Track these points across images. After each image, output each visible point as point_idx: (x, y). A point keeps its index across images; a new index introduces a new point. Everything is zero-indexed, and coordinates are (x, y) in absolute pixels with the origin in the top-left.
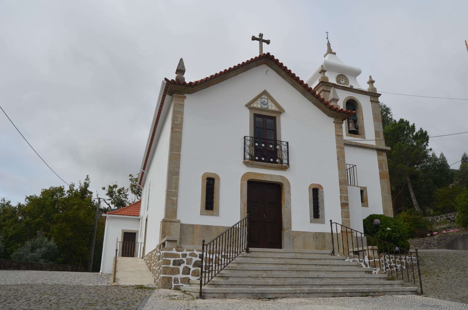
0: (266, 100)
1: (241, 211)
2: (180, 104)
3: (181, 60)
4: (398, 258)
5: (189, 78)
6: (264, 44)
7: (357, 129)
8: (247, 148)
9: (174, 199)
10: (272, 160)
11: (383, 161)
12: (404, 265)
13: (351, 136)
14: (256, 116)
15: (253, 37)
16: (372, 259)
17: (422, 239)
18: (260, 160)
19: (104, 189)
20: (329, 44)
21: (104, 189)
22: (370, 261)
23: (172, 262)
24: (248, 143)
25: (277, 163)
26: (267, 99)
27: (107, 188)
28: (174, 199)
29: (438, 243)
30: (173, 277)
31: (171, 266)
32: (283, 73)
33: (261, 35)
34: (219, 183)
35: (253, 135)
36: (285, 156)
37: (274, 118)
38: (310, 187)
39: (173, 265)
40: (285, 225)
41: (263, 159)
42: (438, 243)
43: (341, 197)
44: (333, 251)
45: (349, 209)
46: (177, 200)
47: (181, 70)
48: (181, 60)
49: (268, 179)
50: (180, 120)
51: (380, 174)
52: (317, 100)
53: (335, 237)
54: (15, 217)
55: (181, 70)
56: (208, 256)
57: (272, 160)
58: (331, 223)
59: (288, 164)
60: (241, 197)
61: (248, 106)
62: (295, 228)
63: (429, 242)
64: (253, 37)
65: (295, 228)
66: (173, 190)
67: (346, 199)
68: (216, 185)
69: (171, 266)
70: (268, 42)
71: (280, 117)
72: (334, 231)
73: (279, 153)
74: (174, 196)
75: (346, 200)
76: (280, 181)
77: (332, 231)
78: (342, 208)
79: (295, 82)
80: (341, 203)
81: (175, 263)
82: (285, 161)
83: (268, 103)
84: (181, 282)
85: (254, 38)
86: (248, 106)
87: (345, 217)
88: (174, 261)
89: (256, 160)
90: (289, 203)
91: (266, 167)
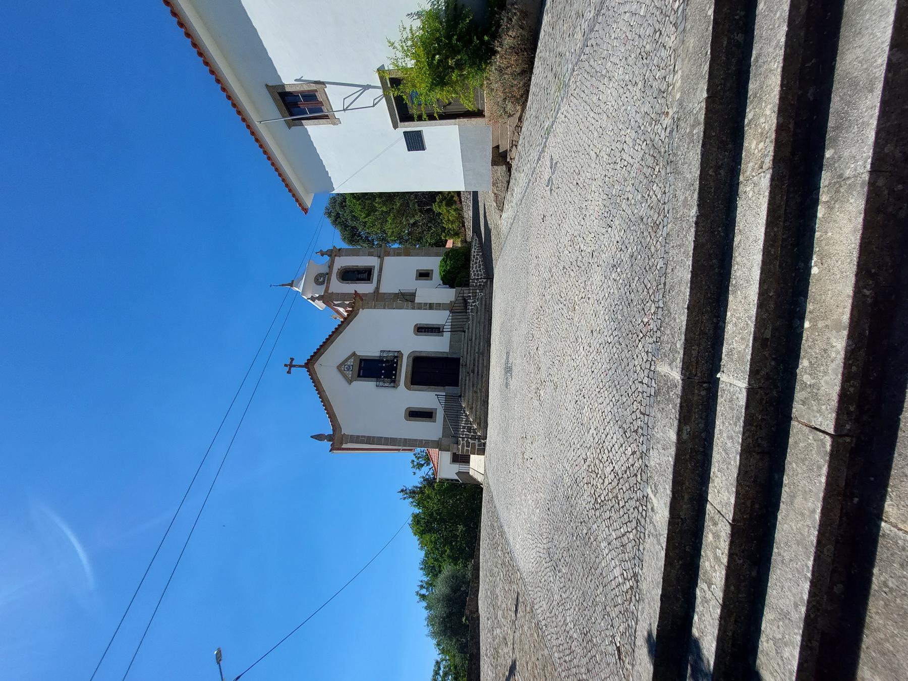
3: (312, 437)
5: (329, 431)
6: (294, 363)
8: (386, 385)
9: (424, 442)
10: (395, 365)
13: (372, 279)
14: (359, 376)
15: (288, 372)
18: (395, 375)
19: (415, 473)
21: (415, 473)
23: (467, 448)
24: (381, 384)
25: (397, 360)
26: (345, 365)
27: (414, 470)
28: (424, 442)
30: (477, 447)
31: (469, 449)
32: (322, 350)
33: (286, 365)
35: (376, 379)
38: (416, 335)
39: (469, 447)
40: (445, 356)
43: (424, 309)
46: (424, 440)
47: (319, 437)
49: (410, 368)
50: (363, 438)
51: (405, 256)
53: (446, 404)
54: (470, 243)
55: (319, 437)
56: (464, 422)
57: (395, 365)
59: (398, 352)
61: (350, 382)
64: (288, 372)
68: (413, 410)
69: (469, 449)
70: (292, 359)
72: (450, 330)
73: (389, 359)
74: (422, 443)
78: (433, 309)
80: (429, 309)
81: (468, 446)
82: (396, 354)
85: (289, 372)
88: (467, 447)
89: (395, 378)
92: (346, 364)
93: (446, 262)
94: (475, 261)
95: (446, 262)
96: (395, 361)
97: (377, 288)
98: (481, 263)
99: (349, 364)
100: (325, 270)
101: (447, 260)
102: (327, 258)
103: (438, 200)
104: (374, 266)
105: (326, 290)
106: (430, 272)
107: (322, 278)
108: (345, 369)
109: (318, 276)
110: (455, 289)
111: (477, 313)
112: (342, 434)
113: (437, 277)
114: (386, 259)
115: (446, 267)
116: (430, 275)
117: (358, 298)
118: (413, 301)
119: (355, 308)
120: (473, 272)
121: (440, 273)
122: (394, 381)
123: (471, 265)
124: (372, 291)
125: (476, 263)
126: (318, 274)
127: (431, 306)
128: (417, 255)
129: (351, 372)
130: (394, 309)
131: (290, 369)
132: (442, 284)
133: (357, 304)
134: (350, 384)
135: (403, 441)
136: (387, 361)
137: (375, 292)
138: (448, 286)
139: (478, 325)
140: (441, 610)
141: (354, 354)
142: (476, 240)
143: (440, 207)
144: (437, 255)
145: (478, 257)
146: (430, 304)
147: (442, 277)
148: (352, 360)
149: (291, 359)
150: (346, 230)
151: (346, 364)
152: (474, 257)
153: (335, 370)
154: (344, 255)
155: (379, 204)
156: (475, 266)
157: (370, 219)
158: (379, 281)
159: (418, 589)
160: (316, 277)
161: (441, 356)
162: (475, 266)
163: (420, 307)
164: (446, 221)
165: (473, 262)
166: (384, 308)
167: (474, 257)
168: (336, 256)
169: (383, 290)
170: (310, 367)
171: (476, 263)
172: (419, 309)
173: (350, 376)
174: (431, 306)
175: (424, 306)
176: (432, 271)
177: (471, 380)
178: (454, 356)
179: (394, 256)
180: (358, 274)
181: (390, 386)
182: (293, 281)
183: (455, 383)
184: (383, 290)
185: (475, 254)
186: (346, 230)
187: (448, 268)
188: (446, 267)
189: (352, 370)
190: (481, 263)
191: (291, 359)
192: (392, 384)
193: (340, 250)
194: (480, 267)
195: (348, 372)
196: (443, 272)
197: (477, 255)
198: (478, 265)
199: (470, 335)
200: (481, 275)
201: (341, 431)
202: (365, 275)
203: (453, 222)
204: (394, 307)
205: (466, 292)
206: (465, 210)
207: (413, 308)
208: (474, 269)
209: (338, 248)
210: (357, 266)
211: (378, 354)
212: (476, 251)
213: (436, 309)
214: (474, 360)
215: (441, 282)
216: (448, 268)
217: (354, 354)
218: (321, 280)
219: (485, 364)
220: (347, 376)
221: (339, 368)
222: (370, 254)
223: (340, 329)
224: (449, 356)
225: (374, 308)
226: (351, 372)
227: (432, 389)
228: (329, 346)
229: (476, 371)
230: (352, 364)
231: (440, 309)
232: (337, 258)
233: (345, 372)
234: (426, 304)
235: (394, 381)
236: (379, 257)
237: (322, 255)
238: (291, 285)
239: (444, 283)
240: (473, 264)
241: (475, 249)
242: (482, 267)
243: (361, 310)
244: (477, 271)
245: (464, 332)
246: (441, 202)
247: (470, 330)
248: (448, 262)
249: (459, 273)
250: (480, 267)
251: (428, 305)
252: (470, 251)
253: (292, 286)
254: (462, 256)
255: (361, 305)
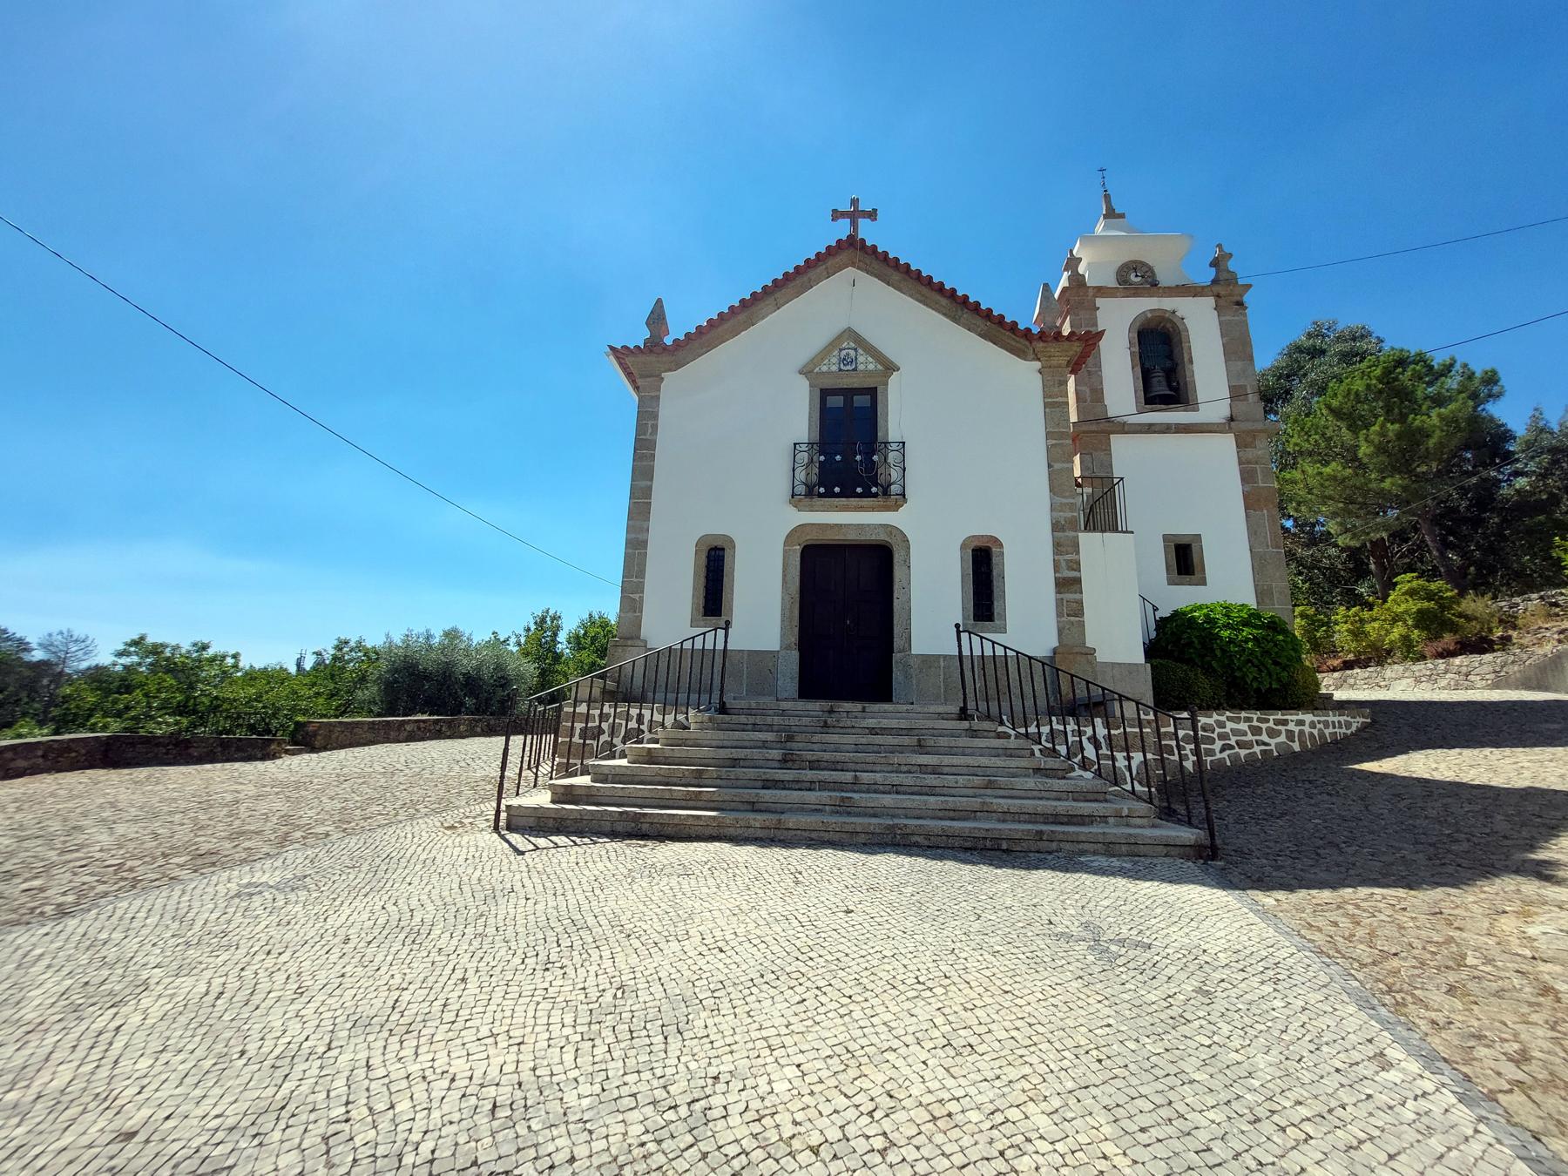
0: (852, 353)
1: (783, 615)
2: (652, 397)
3: (659, 301)
4: (1272, 722)
7: (1177, 390)
9: (636, 596)
11: (1257, 463)
12: (1296, 739)
14: (825, 393)
15: (835, 211)
16: (1119, 728)
17: (1441, 661)
18: (830, 494)
20: (1107, 197)
22: (1112, 732)
24: (803, 457)
25: (875, 495)
26: (855, 350)
28: (636, 596)
29: (1495, 672)
32: (896, 276)
33: (855, 202)
34: (734, 556)
35: (816, 437)
36: (895, 475)
37: (872, 392)
38: (963, 546)
40: (898, 643)
41: (859, 490)
42: (1495, 672)
44: (961, 709)
45: (1081, 593)
46: (641, 598)
48: (659, 301)
49: (852, 537)
51: (1246, 497)
52: (989, 323)
58: (959, 633)
60: (784, 581)
61: (806, 371)
62: (918, 648)
63: (1464, 670)
64: (835, 211)
65: (918, 648)
66: (634, 580)
67: (1075, 567)
70: (872, 215)
71: (886, 384)
72: (966, 652)
75: (1073, 570)
76: (882, 537)
77: (960, 652)
78: (1058, 592)
79: (925, 290)
82: (894, 489)
83: (856, 359)
84: (1261, 728)
86: (806, 371)
87: (1068, 615)
89: (820, 496)
90: (907, 587)
91: (846, 509)
92: (860, 351)
93: (1246, 623)
94: (1264, 726)
95: (1246, 623)
96: (874, 490)
97: (1125, 429)
98: (1257, 749)
99: (861, 359)
100: (1165, 279)
101: (1256, 627)
102: (1206, 276)
103: (1433, 586)
104: (1203, 582)
105: (1102, 291)
106: (1198, 575)
107: (1139, 279)
108: (844, 352)
109: (1145, 269)
110: (1142, 660)
111: (1037, 770)
112: (663, 375)
113: (1184, 598)
114: (1227, 443)
115: (1227, 626)
116: (1188, 578)
117: (1077, 348)
118: (1092, 525)
119: (1040, 345)
120: (1217, 722)
121: (1200, 608)
122: (810, 492)
123: (1243, 714)
124: (1112, 412)
125: (1256, 731)
126: (1151, 269)
127: (1068, 585)
128: (1253, 532)
129: (834, 368)
130: (1050, 466)
131: (844, 215)
132: (1159, 615)
133: (1053, 348)
134: (801, 373)
135: (640, 537)
136: (872, 466)
137: (1108, 419)
138: (1153, 635)
139: (977, 780)
140: (428, 663)
141: (890, 368)
142: (1349, 726)
143: (1412, 593)
144: (1262, 593)
145: (1282, 738)
146: (1078, 581)
147: (1184, 614)
148: (871, 367)
149: (875, 210)
150: (1279, 378)
151: (860, 351)
152: (1277, 722)
153: (843, 325)
154: (1223, 318)
155: (1383, 434)
156: (1244, 726)
157: (1325, 419)
158: (1150, 429)
159: (551, 613)
160: (1141, 262)
161: (897, 629)
162: (1244, 726)
163: (1065, 549)
164: (1356, 615)
165: (1259, 720)
166: (1049, 435)
167: (1277, 722)
168: (1218, 296)
169: (1118, 443)
170: (843, 257)
171: (1256, 731)
172: (1058, 547)
173: (825, 369)
174: (1068, 585)
175: (1067, 561)
176: (1203, 582)
177: (756, 754)
178: (897, 675)
179: (1240, 463)
180: (1163, 370)
181: (796, 483)
182: (1122, 216)
183: (810, 687)
184: (1118, 443)
185: (1291, 726)
186: (1279, 378)
187: (1225, 633)
188: (1227, 626)
189: (840, 370)
190: (1257, 749)
191: (875, 210)
192: (801, 489)
193: (1240, 304)
194: (1240, 744)
195: (834, 360)
196: (1207, 616)
197: (1290, 735)
198: (1250, 737)
199: (943, 741)
200: (1211, 752)
201: (670, 370)
202: (1161, 388)
203: (1357, 634)
204: (1057, 466)
205: (1136, 713)
206: (1415, 668)
207: (1056, 527)
208: (1230, 725)
209: (1245, 299)
210: (1191, 362)
211: (893, 435)
212: (1307, 729)
213: (1059, 603)
214: (835, 766)
215: (1165, 612)
216: (1225, 633)
217: (890, 368)
218: (1132, 277)
219: (792, 820)
220: (823, 359)
221: (851, 334)
222: (1236, 394)
223: (967, 315)
224: (896, 657)
225: (1046, 405)
226: (834, 368)
227: (791, 612)
228: (911, 296)
229: (787, 775)
230: (861, 367)
231: (1059, 614)
232: (1211, 301)
233: (836, 353)
234: (1075, 565)
235: (810, 492)
236: (1232, 419)
237: (1215, 263)
238: (1111, 214)
239: (1162, 624)
240: (1248, 720)
241: (1313, 725)
242: (1243, 753)
243: (1038, 365)
244: (1222, 737)
245: (963, 714)
246: (1430, 596)
247: (964, 741)
248: (1246, 632)
249: (1208, 671)
250: (1240, 744)
251: (1073, 574)
252: (1297, 706)
253: (1105, 217)
254: (1279, 680)
255: (1054, 362)
